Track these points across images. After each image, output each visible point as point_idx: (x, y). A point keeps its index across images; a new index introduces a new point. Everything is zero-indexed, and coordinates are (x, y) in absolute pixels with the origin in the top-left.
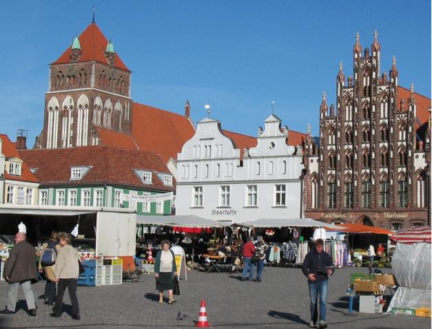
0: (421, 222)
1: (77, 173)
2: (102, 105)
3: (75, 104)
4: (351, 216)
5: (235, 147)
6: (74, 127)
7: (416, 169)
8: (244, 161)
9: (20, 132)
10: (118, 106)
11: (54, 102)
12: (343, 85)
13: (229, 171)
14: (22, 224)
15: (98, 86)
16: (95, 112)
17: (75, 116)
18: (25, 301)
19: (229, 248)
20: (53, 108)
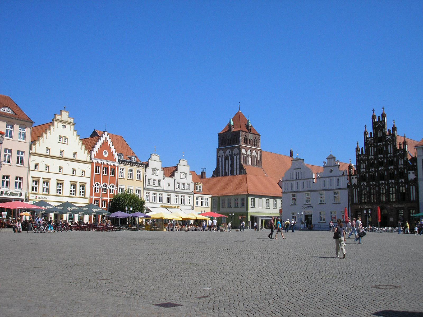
1: (415, 164)
2: (246, 153)
3: (232, 153)
6: (232, 165)
7: (409, 180)
9: (202, 169)
10: (254, 153)
12: (367, 137)
16: (242, 157)
17: (232, 159)
19: (248, 236)
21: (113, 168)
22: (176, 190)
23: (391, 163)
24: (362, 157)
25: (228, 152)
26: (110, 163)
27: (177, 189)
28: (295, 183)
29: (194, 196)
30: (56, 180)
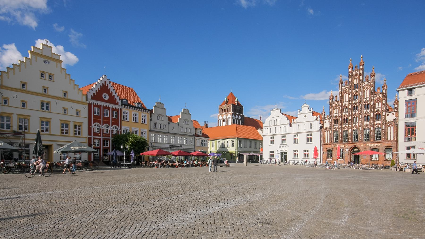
0: (390, 147)
3: (227, 117)
4: (347, 146)
5: (288, 119)
8: (292, 125)
10: (240, 118)
11: (220, 117)
13: (286, 129)
14: (64, 27)
15: (233, 111)
18: (262, 155)
20: (220, 119)
21: (117, 110)
22: (179, 133)
23: (367, 106)
24: (336, 103)
25: (224, 117)
26: (111, 106)
27: (180, 132)
28: (273, 128)
29: (195, 138)
30: (39, 117)
